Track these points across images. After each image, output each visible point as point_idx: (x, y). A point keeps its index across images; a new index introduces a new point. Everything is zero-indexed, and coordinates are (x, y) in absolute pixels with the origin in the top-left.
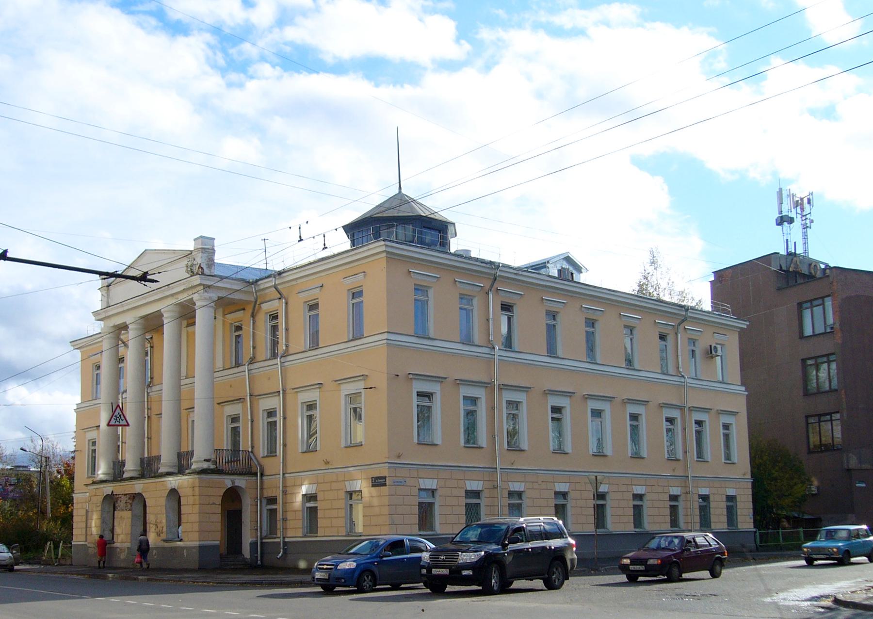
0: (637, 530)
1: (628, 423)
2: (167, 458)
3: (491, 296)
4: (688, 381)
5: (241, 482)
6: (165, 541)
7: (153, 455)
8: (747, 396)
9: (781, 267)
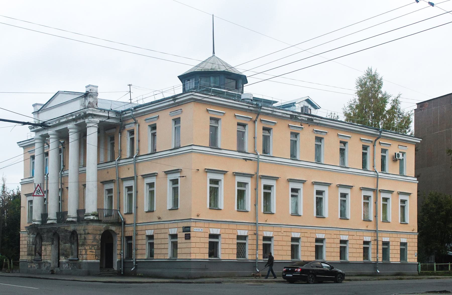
0: (238, 259)
6: (312, 267)
8: (418, 184)
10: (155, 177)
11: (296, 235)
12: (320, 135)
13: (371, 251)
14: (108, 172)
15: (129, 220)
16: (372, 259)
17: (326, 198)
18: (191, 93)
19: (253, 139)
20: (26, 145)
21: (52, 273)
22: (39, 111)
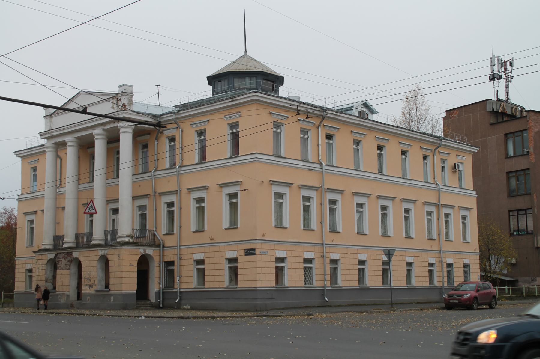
1: (426, 217)
2: (98, 235)
3: (320, 129)
4: (442, 187)
5: (150, 251)
7: (79, 232)
8: (477, 197)
9: (493, 109)
10: (206, 191)
11: (362, 257)
12: (382, 143)
13: (435, 274)
14: (140, 186)
15: (169, 241)
16: (437, 283)
17: (390, 212)
18: (255, 94)
19: (316, 147)
20: (30, 156)
21: (72, 306)
22: (52, 114)
